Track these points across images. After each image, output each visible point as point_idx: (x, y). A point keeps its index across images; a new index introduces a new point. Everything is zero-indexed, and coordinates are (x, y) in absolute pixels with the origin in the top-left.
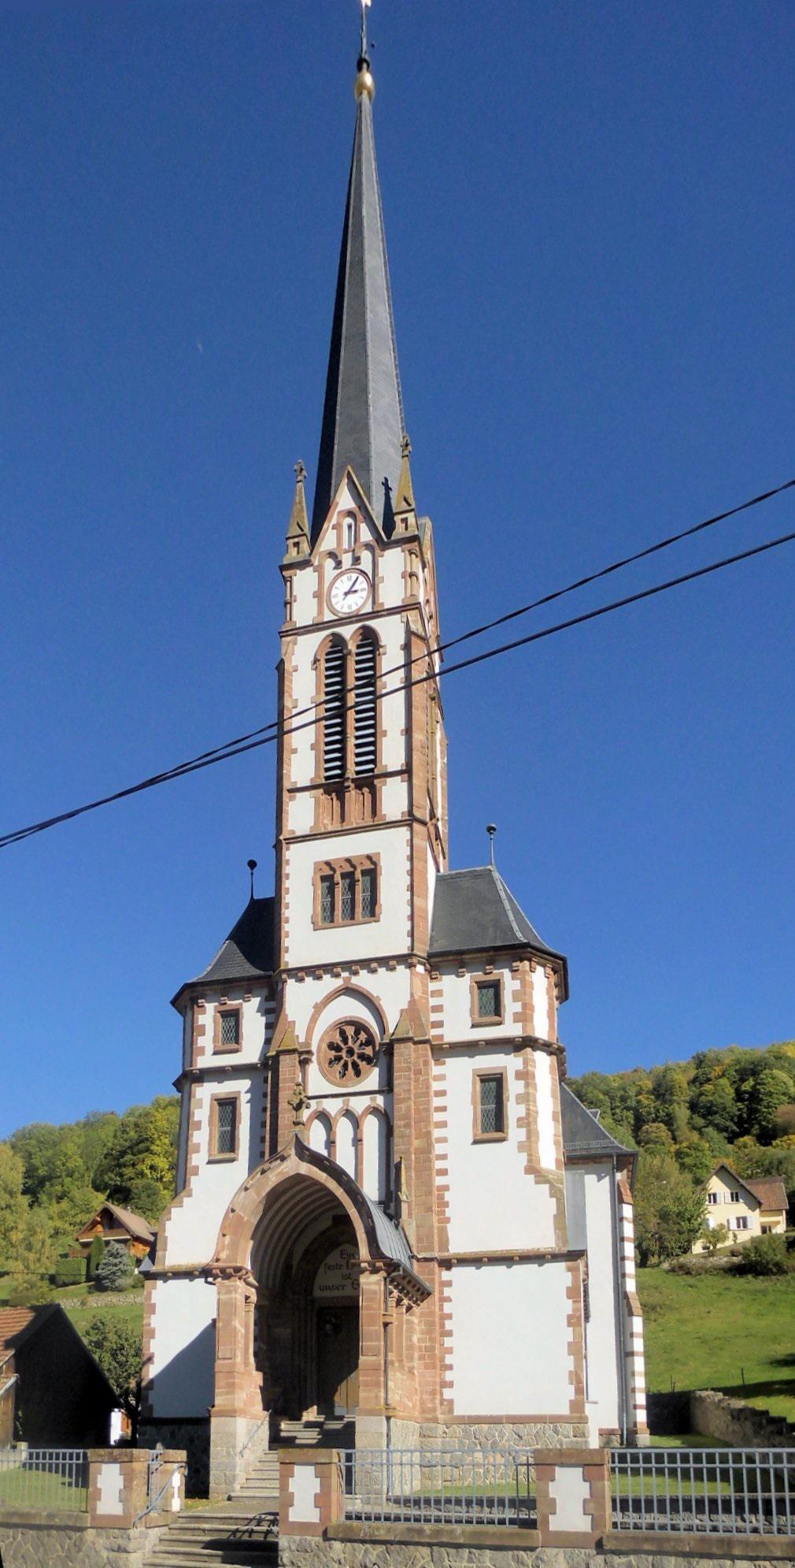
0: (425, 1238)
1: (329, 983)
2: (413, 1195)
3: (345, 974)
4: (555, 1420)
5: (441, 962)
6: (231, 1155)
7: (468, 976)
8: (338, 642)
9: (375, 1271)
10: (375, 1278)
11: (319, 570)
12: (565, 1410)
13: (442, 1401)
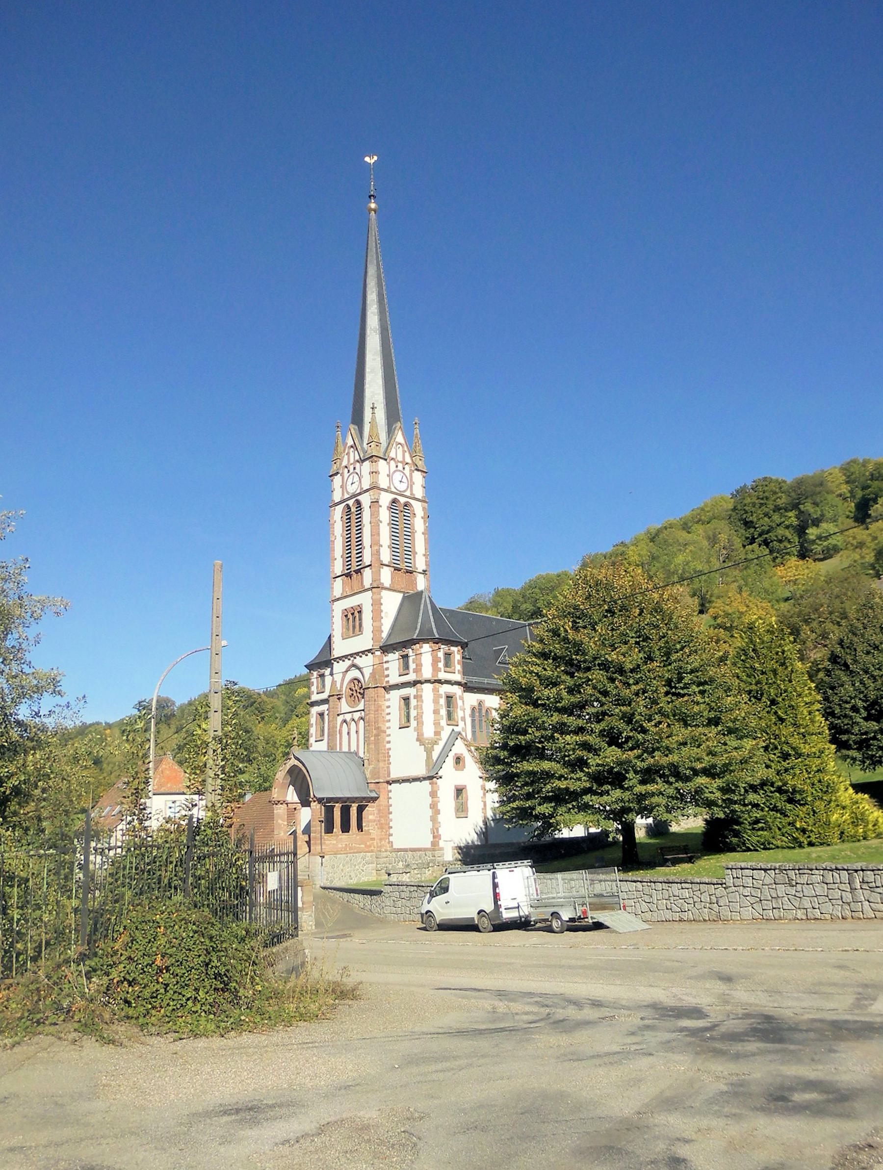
0: (376, 773)
1: (348, 663)
2: (74, 891)
3: (352, 659)
4: (425, 850)
5: (386, 649)
6: (406, 672)
7: (397, 653)
8: (348, 506)
9: (315, 801)
10: (315, 804)
11: (342, 475)
12: (429, 846)
13: (389, 842)
